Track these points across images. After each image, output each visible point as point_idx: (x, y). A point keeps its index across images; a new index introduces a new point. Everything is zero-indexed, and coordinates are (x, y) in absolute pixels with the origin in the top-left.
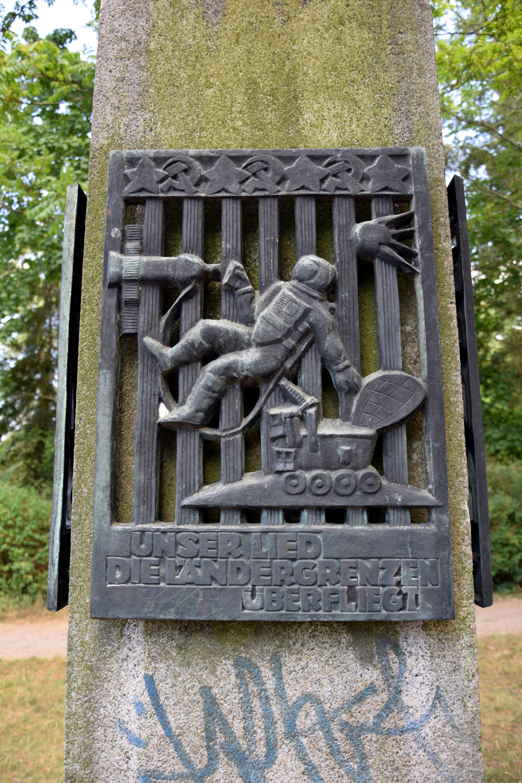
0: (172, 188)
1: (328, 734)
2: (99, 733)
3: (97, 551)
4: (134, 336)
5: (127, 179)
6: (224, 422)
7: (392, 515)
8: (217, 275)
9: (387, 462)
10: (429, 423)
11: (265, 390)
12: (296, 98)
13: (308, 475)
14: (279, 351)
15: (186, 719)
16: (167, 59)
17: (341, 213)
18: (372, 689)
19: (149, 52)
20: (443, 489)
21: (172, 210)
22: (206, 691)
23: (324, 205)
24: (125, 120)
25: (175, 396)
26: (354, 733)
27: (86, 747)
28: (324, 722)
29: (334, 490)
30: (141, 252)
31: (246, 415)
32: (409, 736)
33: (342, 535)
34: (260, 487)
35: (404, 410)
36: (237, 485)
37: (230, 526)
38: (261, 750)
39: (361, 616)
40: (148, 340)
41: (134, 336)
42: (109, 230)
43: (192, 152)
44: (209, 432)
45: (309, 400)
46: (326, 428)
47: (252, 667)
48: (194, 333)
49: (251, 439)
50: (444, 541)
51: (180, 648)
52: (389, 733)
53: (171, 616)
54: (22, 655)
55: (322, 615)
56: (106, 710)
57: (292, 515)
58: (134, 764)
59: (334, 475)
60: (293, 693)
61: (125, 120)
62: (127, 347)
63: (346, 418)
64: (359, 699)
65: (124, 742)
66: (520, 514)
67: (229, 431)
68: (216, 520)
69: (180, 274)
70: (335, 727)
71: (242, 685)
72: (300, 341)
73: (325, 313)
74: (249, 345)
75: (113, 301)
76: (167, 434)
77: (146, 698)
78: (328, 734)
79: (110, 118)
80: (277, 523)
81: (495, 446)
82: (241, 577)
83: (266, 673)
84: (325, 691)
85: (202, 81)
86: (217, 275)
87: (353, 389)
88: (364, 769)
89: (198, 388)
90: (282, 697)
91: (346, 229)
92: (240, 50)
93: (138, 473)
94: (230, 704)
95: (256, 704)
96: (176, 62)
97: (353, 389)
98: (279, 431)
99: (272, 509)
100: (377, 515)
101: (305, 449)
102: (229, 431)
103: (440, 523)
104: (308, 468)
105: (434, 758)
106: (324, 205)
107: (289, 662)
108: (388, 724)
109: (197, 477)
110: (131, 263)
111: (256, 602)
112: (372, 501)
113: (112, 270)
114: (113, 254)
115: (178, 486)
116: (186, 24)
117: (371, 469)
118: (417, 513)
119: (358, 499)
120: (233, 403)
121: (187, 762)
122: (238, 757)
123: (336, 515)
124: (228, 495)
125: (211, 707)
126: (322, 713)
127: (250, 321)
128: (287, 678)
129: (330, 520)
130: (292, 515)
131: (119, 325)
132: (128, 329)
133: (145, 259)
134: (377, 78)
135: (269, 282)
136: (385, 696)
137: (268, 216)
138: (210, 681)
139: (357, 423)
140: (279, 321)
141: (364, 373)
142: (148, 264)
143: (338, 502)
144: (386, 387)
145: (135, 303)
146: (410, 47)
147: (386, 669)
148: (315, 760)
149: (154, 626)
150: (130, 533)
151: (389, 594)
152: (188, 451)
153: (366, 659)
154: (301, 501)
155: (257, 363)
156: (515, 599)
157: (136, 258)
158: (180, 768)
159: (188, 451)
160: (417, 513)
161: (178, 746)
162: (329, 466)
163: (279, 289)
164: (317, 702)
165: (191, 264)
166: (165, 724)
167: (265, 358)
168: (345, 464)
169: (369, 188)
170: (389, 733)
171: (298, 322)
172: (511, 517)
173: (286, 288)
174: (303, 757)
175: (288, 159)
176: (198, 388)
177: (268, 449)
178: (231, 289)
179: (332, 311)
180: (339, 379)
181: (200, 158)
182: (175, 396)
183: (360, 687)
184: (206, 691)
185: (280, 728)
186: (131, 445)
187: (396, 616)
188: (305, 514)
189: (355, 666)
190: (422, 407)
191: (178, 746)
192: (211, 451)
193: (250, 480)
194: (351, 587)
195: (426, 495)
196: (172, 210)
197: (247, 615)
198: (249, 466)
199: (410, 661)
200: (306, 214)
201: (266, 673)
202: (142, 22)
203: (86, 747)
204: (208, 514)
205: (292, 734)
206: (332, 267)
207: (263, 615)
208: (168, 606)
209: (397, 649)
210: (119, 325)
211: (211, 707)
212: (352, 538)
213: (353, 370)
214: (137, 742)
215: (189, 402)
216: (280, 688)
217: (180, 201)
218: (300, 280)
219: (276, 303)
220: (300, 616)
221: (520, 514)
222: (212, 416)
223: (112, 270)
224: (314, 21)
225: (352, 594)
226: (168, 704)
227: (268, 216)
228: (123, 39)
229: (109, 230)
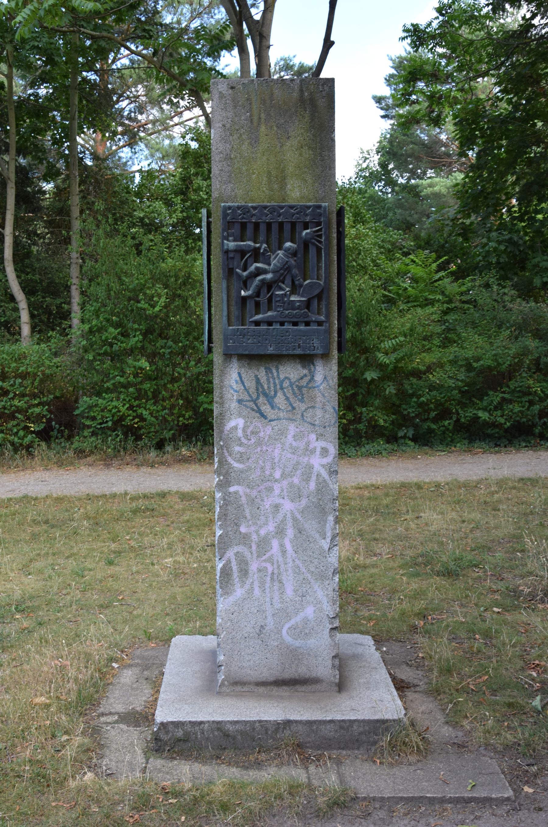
0: (243, 218)
1: (293, 390)
2: (224, 389)
3: (224, 335)
4: (232, 269)
5: (228, 215)
6: (262, 295)
7: (312, 324)
8: (259, 248)
9: (311, 308)
10: (324, 296)
11: (274, 286)
12: (285, 179)
13: (287, 312)
14: (278, 275)
15: (251, 384)
16: (238, 161)
17: (298, 227)
18: (305, 375)
19: (231, 159)
20: (328, 316)
21: (243, 226)
22: (256, 376)
23: (293, 225)
24: (224, 187)
25: (246, 288)
26: (300, 388)
27: (221, 393)
28: (291, 385)
29: (294, 316)
30: (234, 240)
31: (268, 293)
32: (316, 389)
33: (297, 330)
34: (273, 316)
35: (316, 292)
36: (266, 315)
37: (264, 327)
38: (273, 393)
39: (302, 353)
40: (237, 270)
41: (232, 269)
42: (223, 233)
43: (250, 205)
44: (257, 299)
45: (288, 289)
46: (293, 298)
47: (270, 369)
48: (252, 268)
49: (270, 300)
50: (329, 332)
51: (248, 364)
52: (310, 388)
53: (247, 353)
54: (17, 494)
55: (291, 352)
56: (226, 383)
57: (282, 324)
58: (235, 398)
59: (295, 312)
60: (282, 377)
61: (224, 187)
62: (230, 273)
63: (299, 295)
64: (302, 378)
65: (232, 391)
66: (544, 360)
67: (263, 299)
68: (259, 326)
69: (247, 249)
70: (294, 386)
71: (267, 374)
72: (285, 271)
73: (293, 262)
74: (269, 272)
75: (226, 257)
76: (244, 299)
77: (238, 379)
78: (293, 390)
79: (218, 186)
80: (277, 326)
81: (542, 277)
82: (267, 342)
83: (274, 371)
84: (292, 376)
85: (251, 171)
86: (259, 248)
87: (301, 286)
88: (303, 398)
89: (254, 286)
90: (279, 378)
91: (301, 233)
92: (265, 158)
93: (235, 311)
94: (263, 380)
95: (271, 380)
96: (241, 163)
97: (301, 286)
98: (278, 299)
99: (276, 322)
100: (307, 324)
101: (286, 304)
102: (263, 299)
103: (326, 326)
104: (287, 310)
105: (323, 395)
106: (293, 225)
107: (281, 368)
108: (310, 386)
109: (254, 313)
110: (231, 245)
111: (271, 349)
112: (306, 320)
113: (225, 247)
114: (225, 242)
115: (248, 316)
116: (244, 147)
117: (306, 310)
118: (320, 323)
119: (301, 319)
120: (265, 290)
121: (250, 396)
122: (266, 395)
123: (295, 324)
124: (263, 318)
125: (258, 381)
126: (290, 382)
127: (269, 264)
128: (280, 372)
129: (293, 325)
130: (282, 324)
131: (228, 265)
132: (231, 267)
133: (236, 243)
134: (314, 171)
135: (275, 251)
136: (309, 377)
137: (275, 228)
138: (258, 373)
139: (302, 296)
140: (279, 265)
141: (305, 280)
142: (237, 245)
143: (296, 320)
144: (311, 285)
145: (233, 258)
146: (326, 158)
147: (310, 370)
148: (288, 395)
149: (241, 357)
150: (234, 329)
151: (310, 347)
152: (250, 305)
153: (304, 367)
154: (285, 320)
155: (272, 278)
156: (531, 452)
157: (233, 243)
158: (249, 398)
159: (250, 305)
160: (320, 323)
161: (248, 392)
162: (293, 309)
163: (278, 254)
164: (289, 379)
165: (251, 245)
166: (244, 386)
167: (274, 276)
168: (298, 309)
169: (308, 219)
170: (310, 388)
171: (284, 265)
172: (537, 362)
173: (280, 253)
174: (284, 394)
175: (282, 207)
176: (254, 286)
177: (275, 305)
178: (263, 254)
179: (295, 261)
180: (297, 283)
181: (252, 207)
182: (246, 288)
183: (302, 375)
184: (256, 376)
185: (278, 387)
186: (233, 303)
187: (312, 353)
188: (286, 324)
189: (301, 369)
190: (322, 291)
191: (248, 392)
192: (257, 305)
193: (270, 313)
194: (299, 344)
195: (322, 318)
196: (243, 226)
197: (269, 352)
198: (270, 309)
199: (317, 367)
200: (287, 228)
201: (274, 371)
202: (228, 145)
203: (221, 393)
204: (257, 323)
205: (282, 388)
206: (295, 246)
207: (273, 352)
208: (246, 350)
209: (314, 365)
210: (228, 265)
211: (258, 381)
212: (300, 330)
213: (301, 280)
214: (236, 391)
215: (251, 289)
216: (278, 375)
217: (245, 223)
218: (285, 251)
219: (278, 258)
220: (285, 353)
221: (544, 360)
222: (258, 294)
223: (225, 247)
224: (292, 146)
225: (299, 346)
226: (245, 381)
227: (275, 228)
228: (221, 152)
229: (223, 233)
